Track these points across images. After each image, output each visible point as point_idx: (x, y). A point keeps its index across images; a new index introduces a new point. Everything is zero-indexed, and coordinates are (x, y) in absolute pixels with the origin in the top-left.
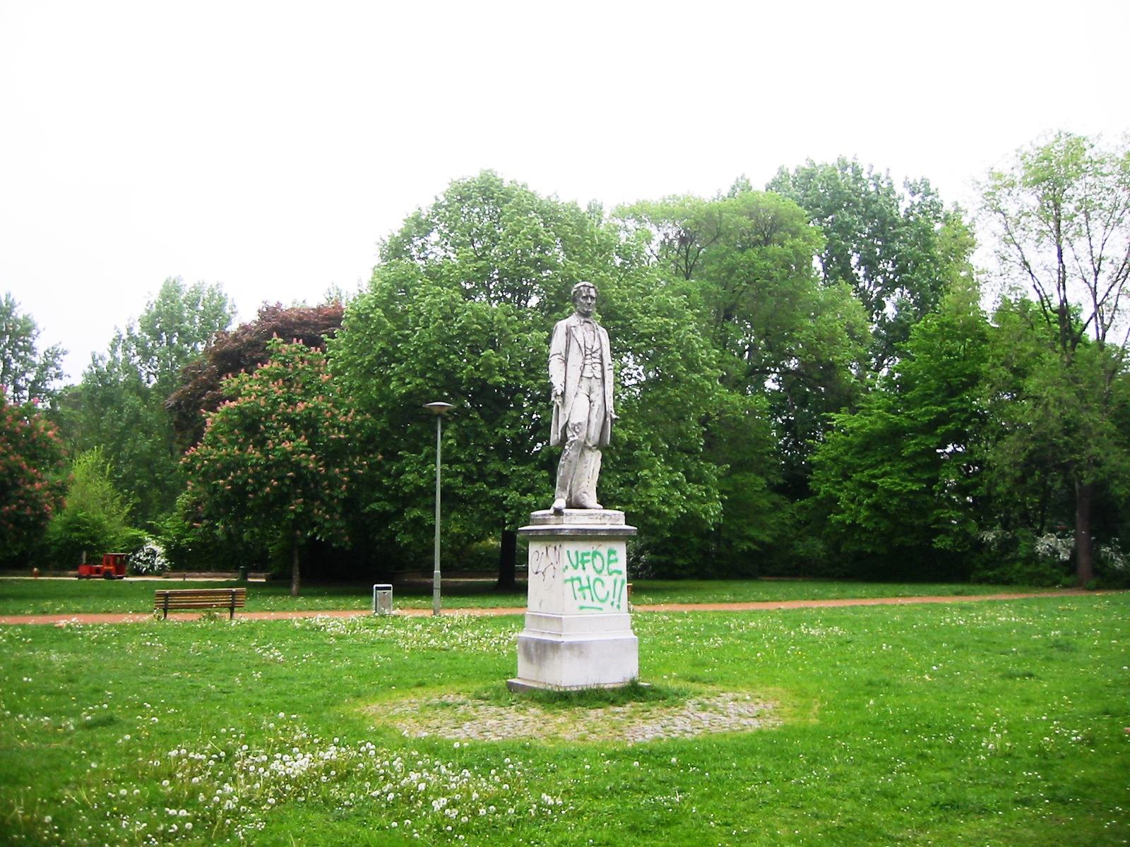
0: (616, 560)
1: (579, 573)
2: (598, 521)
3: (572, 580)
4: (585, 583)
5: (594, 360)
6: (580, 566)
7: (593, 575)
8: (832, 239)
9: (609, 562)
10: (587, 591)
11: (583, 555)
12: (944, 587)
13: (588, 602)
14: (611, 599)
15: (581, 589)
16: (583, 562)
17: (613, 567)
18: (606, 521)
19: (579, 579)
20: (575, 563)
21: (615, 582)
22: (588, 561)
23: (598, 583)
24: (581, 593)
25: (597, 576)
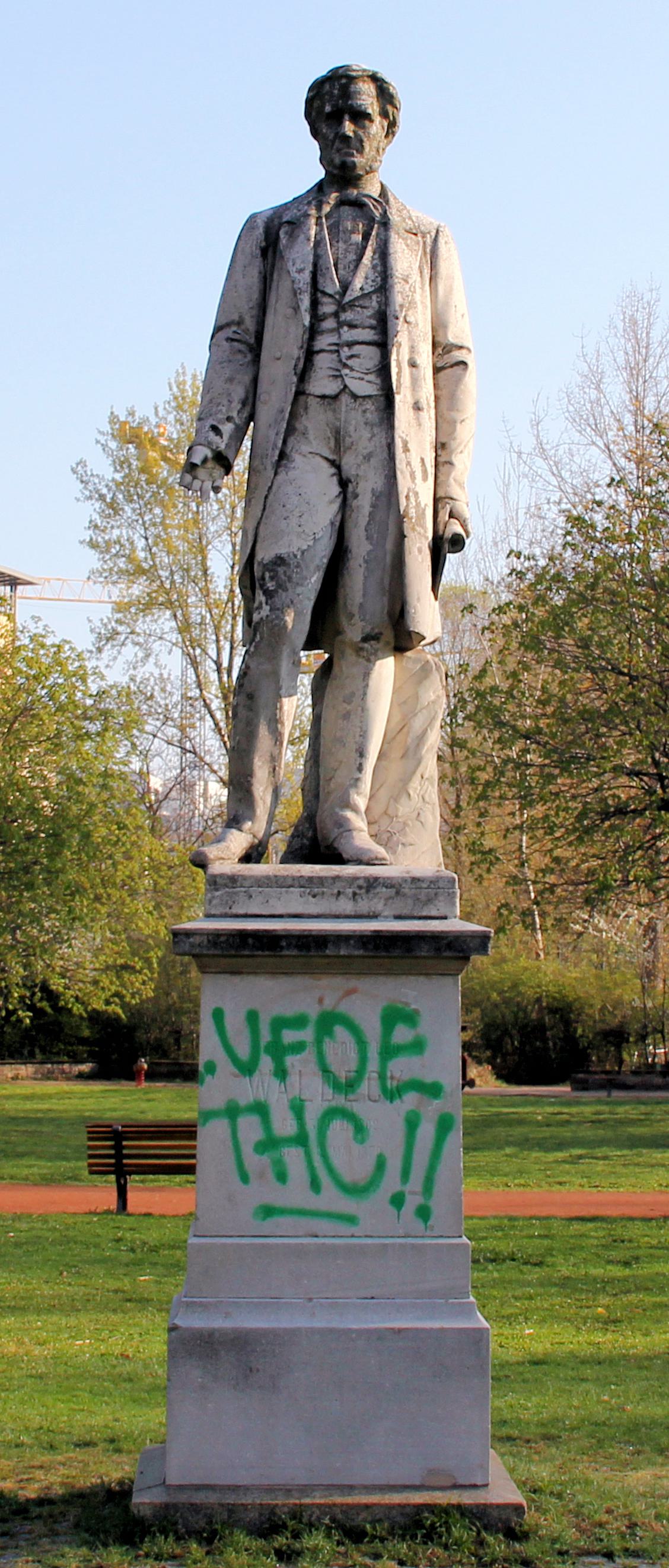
0: (417, 1046)
1: (263, 1085)
2: (345, 905)
3: (232, 1112)
4: (284, 1125)
5: (347, 334)
6: (266, 1063)
7: (318, 1096)
8: (148, 680)
9: (388, 1052)
10: (293, 1156)
11: (279, 1024)
12: (157, 1084)
13: (278, 1196)
14: (391, 1182)
15: (270, 1143)
16: (278, 1051)
17: (402, 1067)
18: (378, 906)
19: (261, 1109)
20: (244, 1052)
21: (412, 1124)
22: (298, 1047)
23: (339, 1129)
24: (265, 1159)
25: (340, 1101)
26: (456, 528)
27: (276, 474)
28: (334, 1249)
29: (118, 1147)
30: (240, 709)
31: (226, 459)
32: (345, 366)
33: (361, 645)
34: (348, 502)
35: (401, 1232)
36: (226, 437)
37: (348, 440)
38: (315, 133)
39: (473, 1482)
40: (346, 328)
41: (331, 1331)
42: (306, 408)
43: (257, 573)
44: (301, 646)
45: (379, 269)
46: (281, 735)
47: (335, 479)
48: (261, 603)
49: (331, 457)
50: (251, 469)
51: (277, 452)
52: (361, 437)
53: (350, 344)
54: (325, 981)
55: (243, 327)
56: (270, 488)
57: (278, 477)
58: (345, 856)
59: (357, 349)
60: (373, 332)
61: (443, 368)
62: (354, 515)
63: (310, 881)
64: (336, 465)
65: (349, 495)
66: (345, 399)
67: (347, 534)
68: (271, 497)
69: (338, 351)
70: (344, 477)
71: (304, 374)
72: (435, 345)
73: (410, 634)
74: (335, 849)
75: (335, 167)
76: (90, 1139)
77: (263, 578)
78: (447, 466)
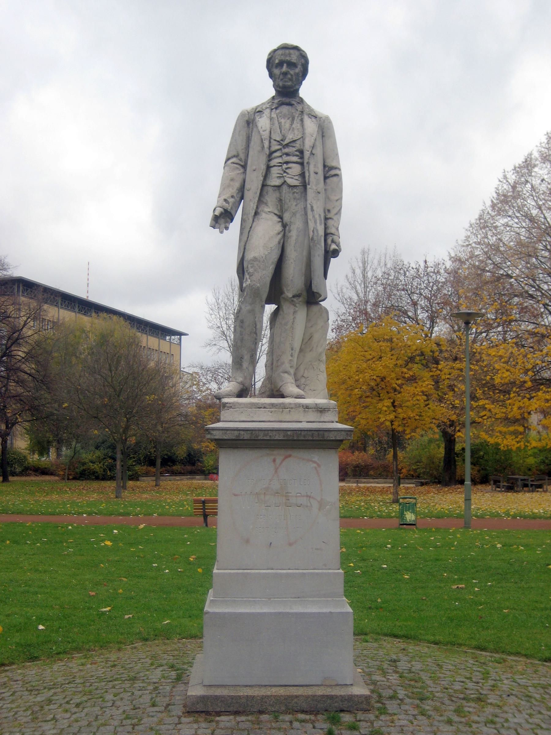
26: (334, 246)
27: (253, 221)
28: (281, 575)
29: (204, 506)
30: (237, 327)
31: (230, 213)
32: (285, 172)
33: (293, 299)
34: (286, 234)
35: (312, 567)
36: (230, 204)
37: (286, 206)
38: (271, 75)
39: (345, 683)
40: (285, 156)
41: (280, 613)
42: (267, 193)
43: (245, 266)
44: (265, 296)
45: (300, 130)
46: (546, 662)
47: (280, 224)
48: (247, 279)
49: (278, 214)
50: (243, 221)
51: (254, 211)
52: (292, 205)
53: (287, 163)
54: (275, 452)
55: (239, 158)
56: (251, 227)
57: (255, 223)
58: (285, 394)
59: (290, 165)
60: (297, 158)
61: (328, 177)
62: (289, 240)
63: (273, 405)
64: (281, 217)
65: (287, 231)
66: (285, 187)
67: (285, 248)
68: (251, 231)
69: (281, 166)
70: (284, 223)
71: (266, 176)
72: (325, 166)
73: (313, 293)
74: (281, 391)
75: (280, 87)
76: (195, 503)
77: (248, 267)
78: (335, 179)
